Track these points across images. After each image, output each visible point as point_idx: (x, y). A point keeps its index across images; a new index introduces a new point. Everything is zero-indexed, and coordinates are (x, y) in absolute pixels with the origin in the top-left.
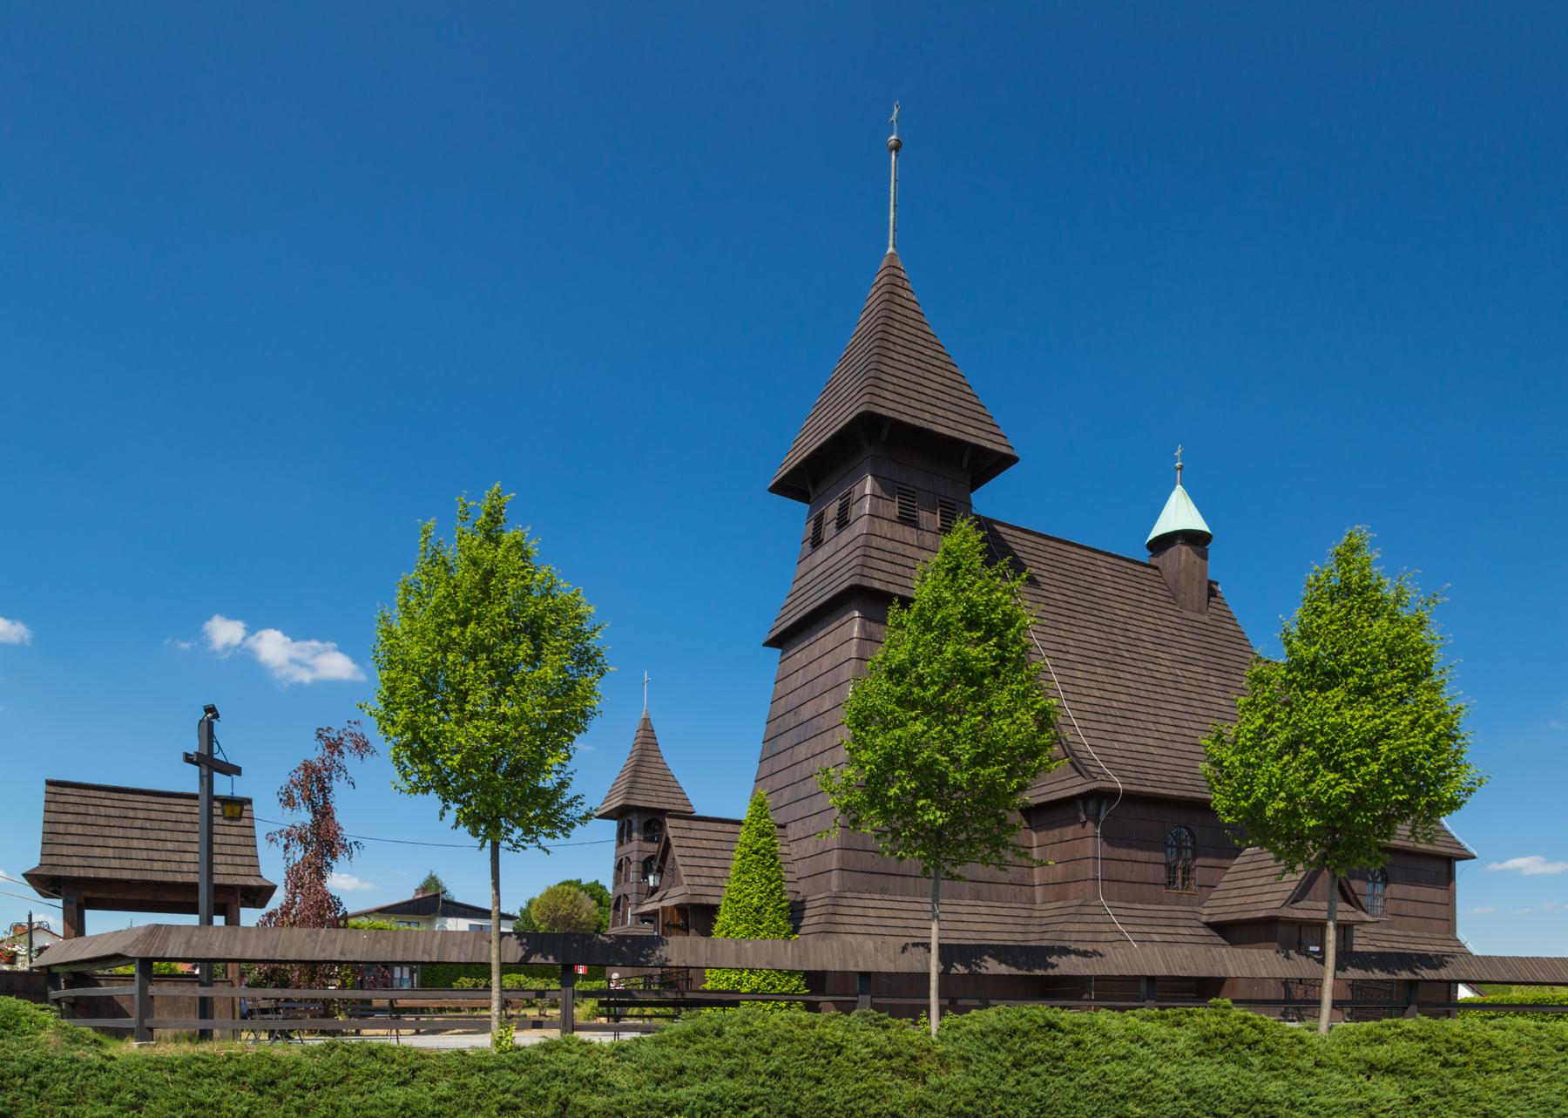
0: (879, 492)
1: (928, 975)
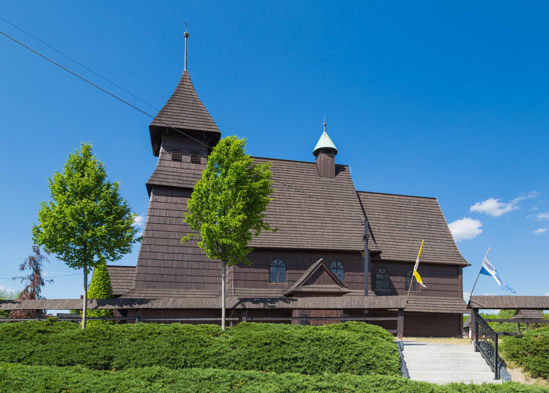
0: (164, 151)
1: (221, 309)
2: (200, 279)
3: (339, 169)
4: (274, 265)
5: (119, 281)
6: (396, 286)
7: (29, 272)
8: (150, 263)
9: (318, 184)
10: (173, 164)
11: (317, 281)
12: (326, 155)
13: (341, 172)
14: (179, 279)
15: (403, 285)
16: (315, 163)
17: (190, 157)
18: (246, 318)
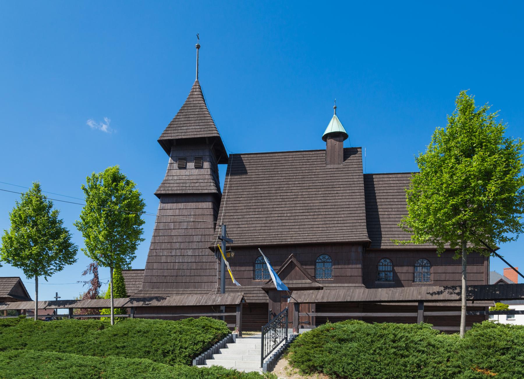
0: (173, 162)
2: (198, 279)
3: (348, 153)
4: (259, 262)
5: (137, 283)
6: (402, 277)
7: (90, 276)
8: (155, 266)
10: (179, 172)
11: (286, 278)
12: (333, 140)
13: (352, 156)
15: (410, 277)
17: (194, 164)
18: (422, 311)
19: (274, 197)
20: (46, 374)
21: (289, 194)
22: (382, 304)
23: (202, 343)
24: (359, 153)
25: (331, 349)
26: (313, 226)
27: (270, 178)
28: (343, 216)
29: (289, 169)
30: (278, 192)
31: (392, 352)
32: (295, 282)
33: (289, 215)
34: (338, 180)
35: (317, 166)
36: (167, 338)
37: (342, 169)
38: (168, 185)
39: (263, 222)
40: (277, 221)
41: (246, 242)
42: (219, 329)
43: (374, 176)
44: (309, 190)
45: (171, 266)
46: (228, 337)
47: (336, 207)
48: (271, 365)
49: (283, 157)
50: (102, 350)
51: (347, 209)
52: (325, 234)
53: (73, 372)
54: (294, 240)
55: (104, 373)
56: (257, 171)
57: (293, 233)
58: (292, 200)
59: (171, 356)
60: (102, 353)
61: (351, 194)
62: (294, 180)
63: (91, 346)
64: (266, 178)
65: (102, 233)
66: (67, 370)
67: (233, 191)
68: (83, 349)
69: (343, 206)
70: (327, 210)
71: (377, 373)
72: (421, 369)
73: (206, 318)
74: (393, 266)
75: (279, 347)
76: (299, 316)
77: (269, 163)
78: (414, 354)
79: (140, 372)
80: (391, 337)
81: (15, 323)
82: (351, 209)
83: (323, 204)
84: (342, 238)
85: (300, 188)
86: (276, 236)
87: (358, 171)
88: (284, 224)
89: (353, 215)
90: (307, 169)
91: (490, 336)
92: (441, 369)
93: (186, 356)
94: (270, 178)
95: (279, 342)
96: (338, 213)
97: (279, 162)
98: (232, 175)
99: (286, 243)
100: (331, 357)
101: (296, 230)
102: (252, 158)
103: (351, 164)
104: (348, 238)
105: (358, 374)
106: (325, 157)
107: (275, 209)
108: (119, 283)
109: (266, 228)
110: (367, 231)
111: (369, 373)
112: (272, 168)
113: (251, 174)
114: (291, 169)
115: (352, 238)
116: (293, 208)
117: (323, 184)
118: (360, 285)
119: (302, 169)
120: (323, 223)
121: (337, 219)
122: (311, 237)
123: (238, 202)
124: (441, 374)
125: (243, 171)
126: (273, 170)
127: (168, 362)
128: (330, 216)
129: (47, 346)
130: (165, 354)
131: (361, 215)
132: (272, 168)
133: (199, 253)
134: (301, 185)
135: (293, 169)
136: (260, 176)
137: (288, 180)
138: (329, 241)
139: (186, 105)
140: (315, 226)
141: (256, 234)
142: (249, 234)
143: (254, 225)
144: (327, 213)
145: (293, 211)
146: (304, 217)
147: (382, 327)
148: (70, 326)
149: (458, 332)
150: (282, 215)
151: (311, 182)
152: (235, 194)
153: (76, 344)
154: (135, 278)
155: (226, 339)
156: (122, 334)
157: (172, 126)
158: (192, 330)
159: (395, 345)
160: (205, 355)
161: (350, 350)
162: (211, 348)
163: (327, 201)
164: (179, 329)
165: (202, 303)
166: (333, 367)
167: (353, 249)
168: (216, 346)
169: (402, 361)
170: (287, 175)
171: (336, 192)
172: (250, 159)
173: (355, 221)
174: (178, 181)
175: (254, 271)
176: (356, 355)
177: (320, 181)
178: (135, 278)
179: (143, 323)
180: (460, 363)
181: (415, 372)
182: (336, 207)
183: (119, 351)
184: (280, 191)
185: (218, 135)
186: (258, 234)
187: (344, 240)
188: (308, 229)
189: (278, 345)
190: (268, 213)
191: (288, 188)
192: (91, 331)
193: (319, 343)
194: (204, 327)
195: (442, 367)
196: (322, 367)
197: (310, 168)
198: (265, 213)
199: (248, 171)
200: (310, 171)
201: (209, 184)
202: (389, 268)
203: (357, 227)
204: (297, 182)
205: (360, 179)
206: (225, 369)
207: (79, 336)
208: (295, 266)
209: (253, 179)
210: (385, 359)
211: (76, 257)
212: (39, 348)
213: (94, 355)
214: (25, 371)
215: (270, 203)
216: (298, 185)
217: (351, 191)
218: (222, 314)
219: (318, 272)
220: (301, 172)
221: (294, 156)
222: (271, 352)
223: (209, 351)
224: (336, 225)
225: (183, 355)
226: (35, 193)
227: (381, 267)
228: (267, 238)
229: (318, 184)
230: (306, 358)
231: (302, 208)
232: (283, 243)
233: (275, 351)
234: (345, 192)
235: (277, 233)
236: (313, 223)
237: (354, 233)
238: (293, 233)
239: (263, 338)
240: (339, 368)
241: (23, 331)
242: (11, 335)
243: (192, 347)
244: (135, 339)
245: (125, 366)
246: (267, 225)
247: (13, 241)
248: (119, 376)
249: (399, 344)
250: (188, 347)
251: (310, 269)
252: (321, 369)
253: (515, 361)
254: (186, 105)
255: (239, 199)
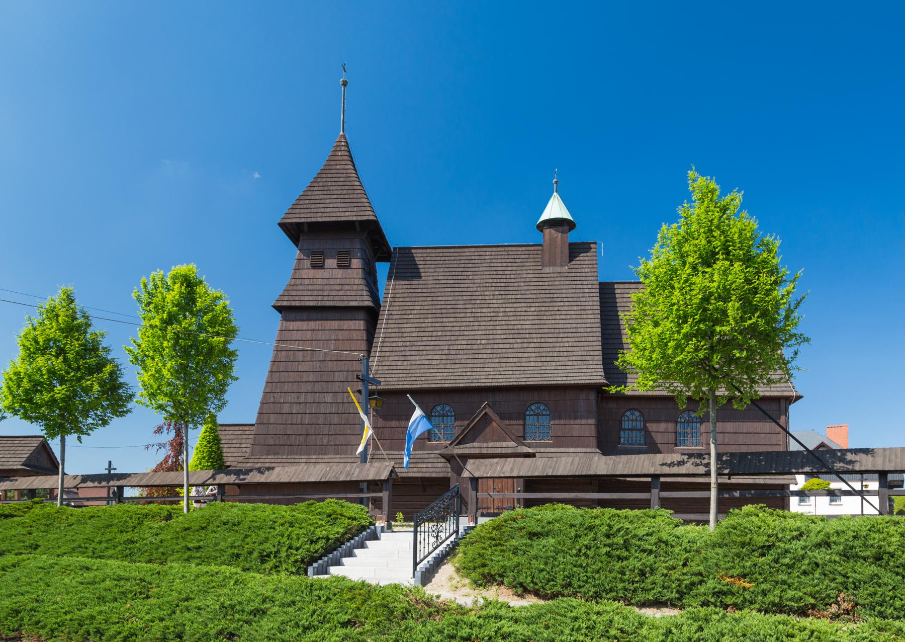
3: (576, 250)
4: (437, 414)
6: (659, 439)
8: (273, 419)
9: (535, 280)
10: (312, 273)
12: (553, 231)
14: (311, 440)
15: (671, 438)
16: (541, 245)
17: (336, 261)
19: (462, 315)
20: (59, 594)
21: (484, 310)
22: (628, 479)
23: (324, 541)
24: (592, 250)
25: (517, 549)
26: (520, 360)
27: (456, 285)
28: (567, 344)
29: (486, 273)
30: (467, 306)
31: (603, 553)
32: (491, 444)
33: (483, 342)
34: (561, 291)
35: (528, 268)
36: (269, 533)
37: (566, 275)
38: (294, 293)
39: (444, 352)
40: (465, 352)
41: (416, 383)
42: (354, 519)
43: (616, 286)
44: (515, 305)
45: (297, 419)
46: (369, 531)
47: (557, 331)
48: (427, 574)
49: (476, 254)
50: (163, 554)
51: (573, 335)
52: (539, 372)
53: (105, 590)
54: (491, 381)
55: (155, 590)
56: (435, 274)
57: (489, 369)
58: (489, 319)
59: (272, 562)
60: (163, 557)
61: (579, 312)
62: (493, 289)
63: (146, 548)
64: (449, 286)
65: (169, 365)
66: (97, 586)
67: (398, 304)
68: (132, 552)
69: (567, 330)
70: (543, 336)
71: (582, 584)
72: (646, 578)
73: (336, 501)
74: (645, 422)
75: (444, 545)
76: (477, 499)
77: (455, 262)
78: (637, 555)
79: (214, 587)
80: (604, 529)
81: (23, 512)
82: (579, 335)
83: (536, 327)
84: (565, 378)
85: (502, 301)
86: (464, 374)
87: (590, 278)
88: (476, 356)
89: (582, 344)
90: (514, 272)
91: (745, 528)
92: (673, 578)
93: (296, 561)
94: (456, 285)
95: (444, 538)
96: (560, 340)
97: (470, 262)
98: (396, 279)
99: (479, 384)
100: (516, 559)
101: (494, 365)
102: (428, 255)
103: (581, 266)
104: (574, 378)
105: (554, 586)
106: (540, 256)
107: (462, 333)
108: (212, 447)
109: (448, 362)
110: (604, 369)
111: (570, 585)
112: (459, 270)
113: (426, 278)
114: (489, 273)
115: (580, 378)
116: (491, 332)
117: (538, 296)
118: (594, 450)
119: (506, 272)
120: (537, 355)
121: (557, 349)
122: (518, 376)
123: (405, 321)
124: (674, 586)
125: (415, 274)
126: (460, 274)
127: (267, 570)
128: (548, 345)
129: (73, 549)
130: (264, 558)
131: (595, 344)
132: (459, 270)
133: (343, 400)
134: (504, 297)
135: (492, 273)
136: (440, 282)
137: (484, 289)
138: (545, 383)
139: (324, 171)
140: (524, 360)
141: (432, 371)
142: (422, 371)
143: (430, 357)
144: (543, 340)
145: (491, 337)
146: (508, 346)
147: (593, 514)
148: (112, 516)
149: (707, 522)
150: (474, 342)
151: (519, 292)
152: (401, 308)
153: (120, 544)
154: (240, 437)
155: (364, 533)
156: (197, 528)
157: (301, 202)
158: (310, 519)
159: (609, 541)
160: (328, 559)
161: (544, 550)
162: (340, 547)
163: (542, 322)
164: (289, 518)
165: (330, 477)
166: (518, 576)
167: (583, 395)
168: (348, 544)
169: (618, 565)
170: (482, 281)
171: (556, 308)
172: (425, 255)
173: (585, 353)
174: (310, 287)
175: (524, 425)
176: (552, 557)
177: (532, 292)
178: (240, 437)
179: (235, 510)
180: (701, 568)
181: (637, 582)
182: (557, 331)
183: (191, 554)
184: (470, 306)
185: (374, 218)
186: (436, 371)
187: (568, 382)
188: (513, 365)
189: (441, 543)
190: (453, 338)
191: (483, 302)
192: (147, 523)
193: (500, 539)
194: (330, 516)
195: (675, 575)
196: (501, 576)
197: (518, 272)
198: (448, 338)
199: (423, 274)
200: (518, 276)
201: (360, 293)
202: (640, 425)
203: (587, 363)
204: (497, 293)
205: (593, 290)
206: (350, 580)
207: (127, 532)
208: (492, 420)
209: (430, 286)
210: (594, 563)
211: (129, 406)
212: (59, 552)
213: (150, 561)
214: (24, 589)
215: (455, 324)
216: (500, 297)
217: (579, 308)
218: (361, 495)
219: (528, 430)
220: (504, 277)
221: (494, 253)
222: (430, 554)
223: (335, 553)
224: (556, 359)
225: (292, 559)
226: (64, 304)
227: (626, 423)
228: (449, 378)
229: (530, 296)
230: (479, 562)
231: (504, 332)
232: (474, 385)
233: (437, 551)
234: (570, 308)
235: (464, 370)
236: (520, 355)
237: (583, 371)
238: (489, 369)
239: (415, 532)
240: (526, 578)
241: (34, 524)
242: (13, 532)
243: (306, 546)
244: (217, 536)
245: (192, 578)
246: (450, 357)
247: (23, 378)
248: (180, 593)
249: (615, 540)
250: (301, 547)
251: (515, 426)
252: (500, 579)
253: (777, 565)
254: (324, 171)
255: (406, 317)
